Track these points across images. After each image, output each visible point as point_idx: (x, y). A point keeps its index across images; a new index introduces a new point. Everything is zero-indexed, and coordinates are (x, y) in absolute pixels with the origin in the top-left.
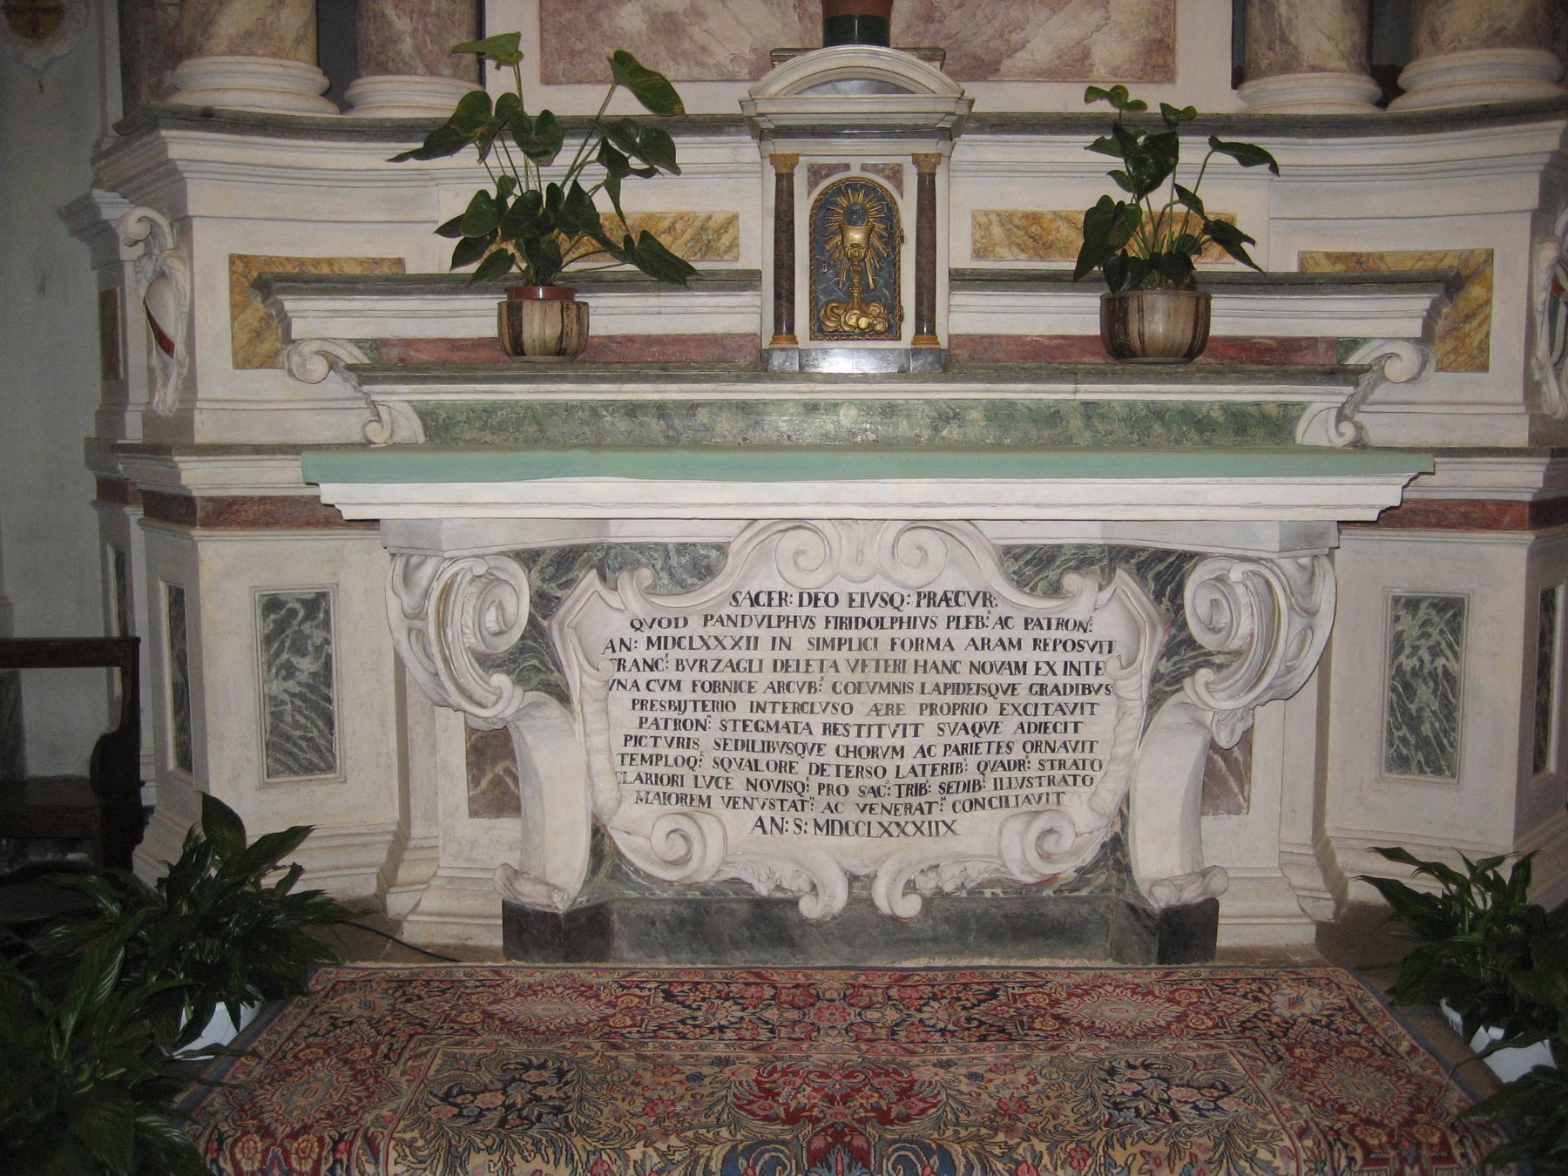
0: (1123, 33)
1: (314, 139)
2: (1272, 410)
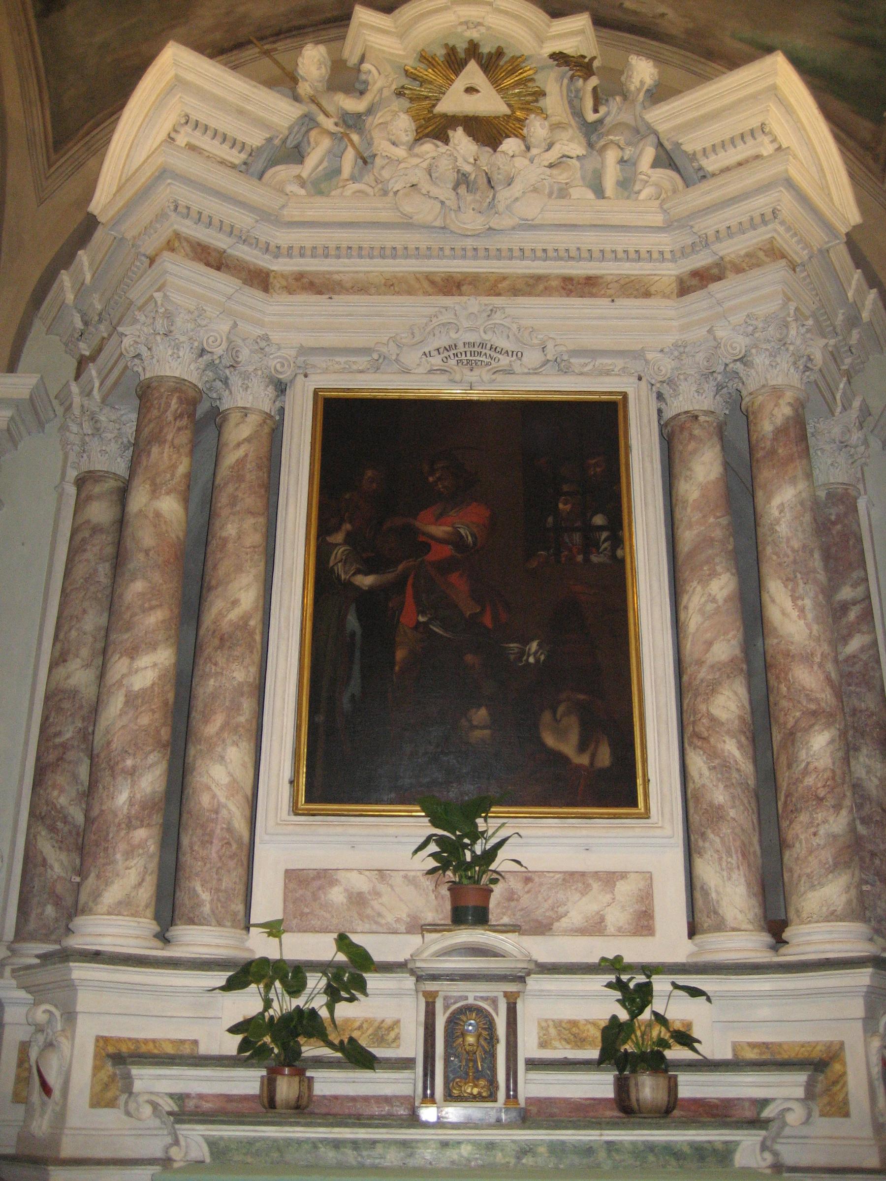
0: (623, 907)
1: (154, 968)
2: (720, 1147)
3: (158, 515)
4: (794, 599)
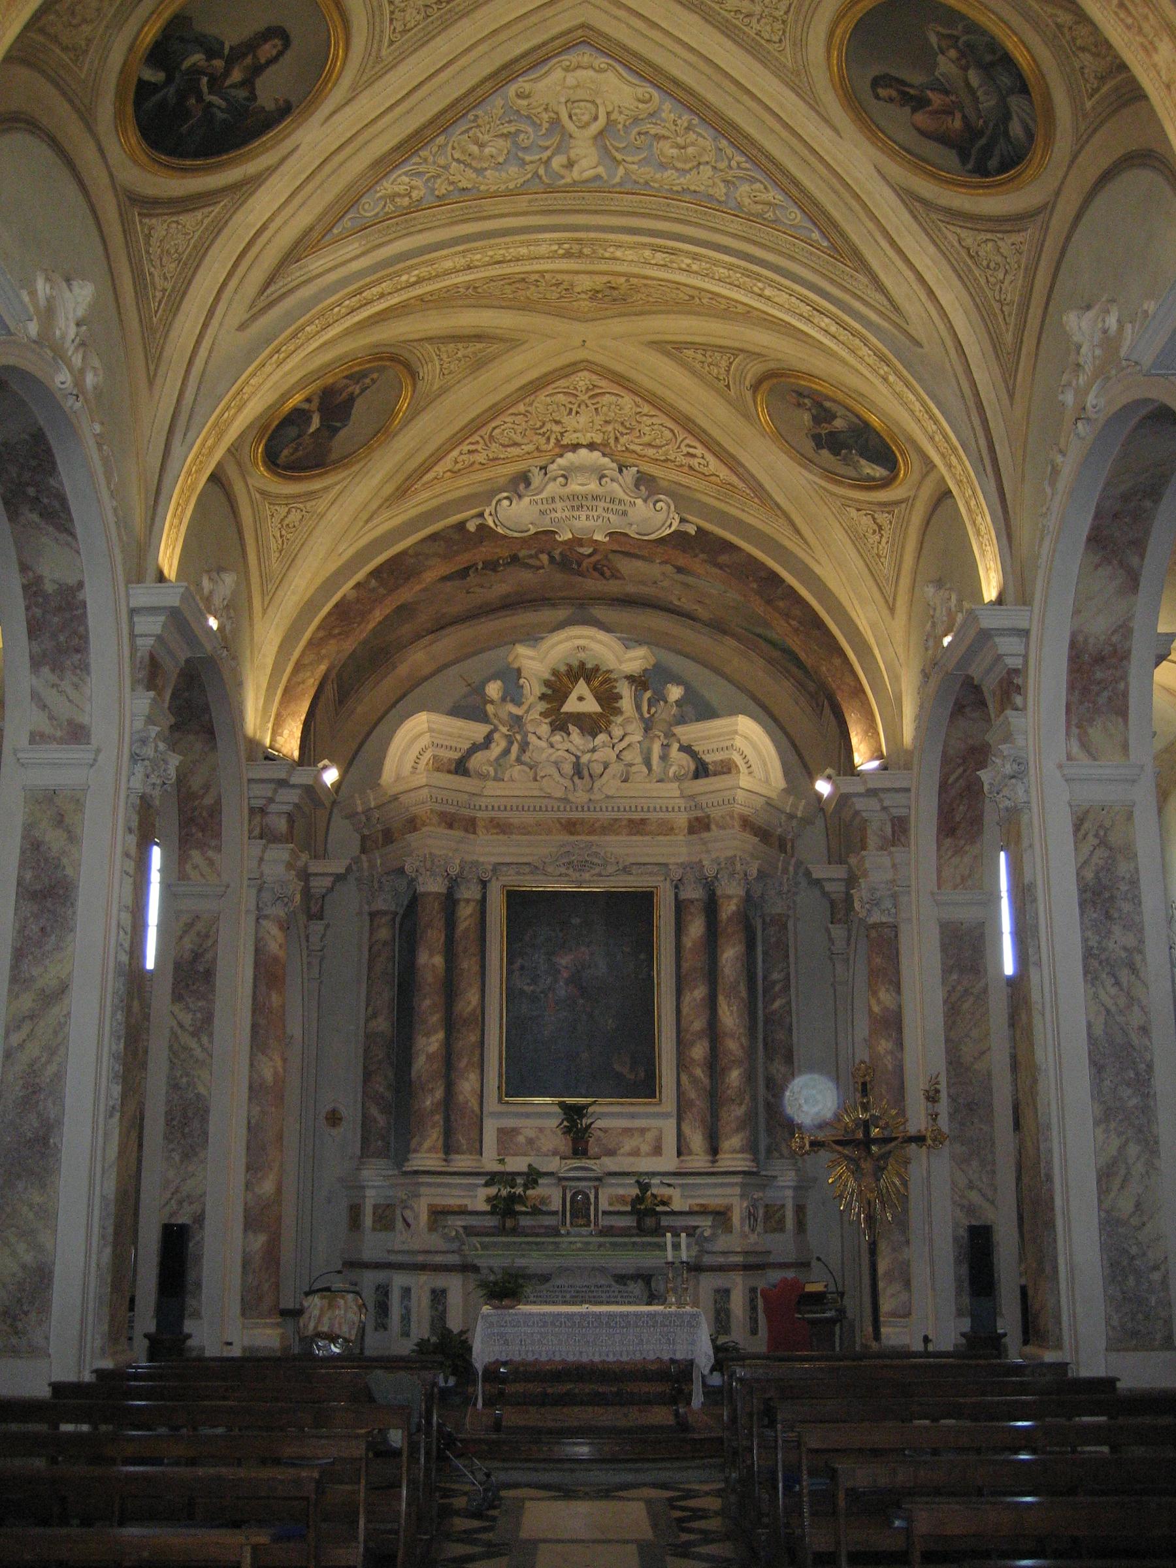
3: (433, 966)
4: (729, 1006)
